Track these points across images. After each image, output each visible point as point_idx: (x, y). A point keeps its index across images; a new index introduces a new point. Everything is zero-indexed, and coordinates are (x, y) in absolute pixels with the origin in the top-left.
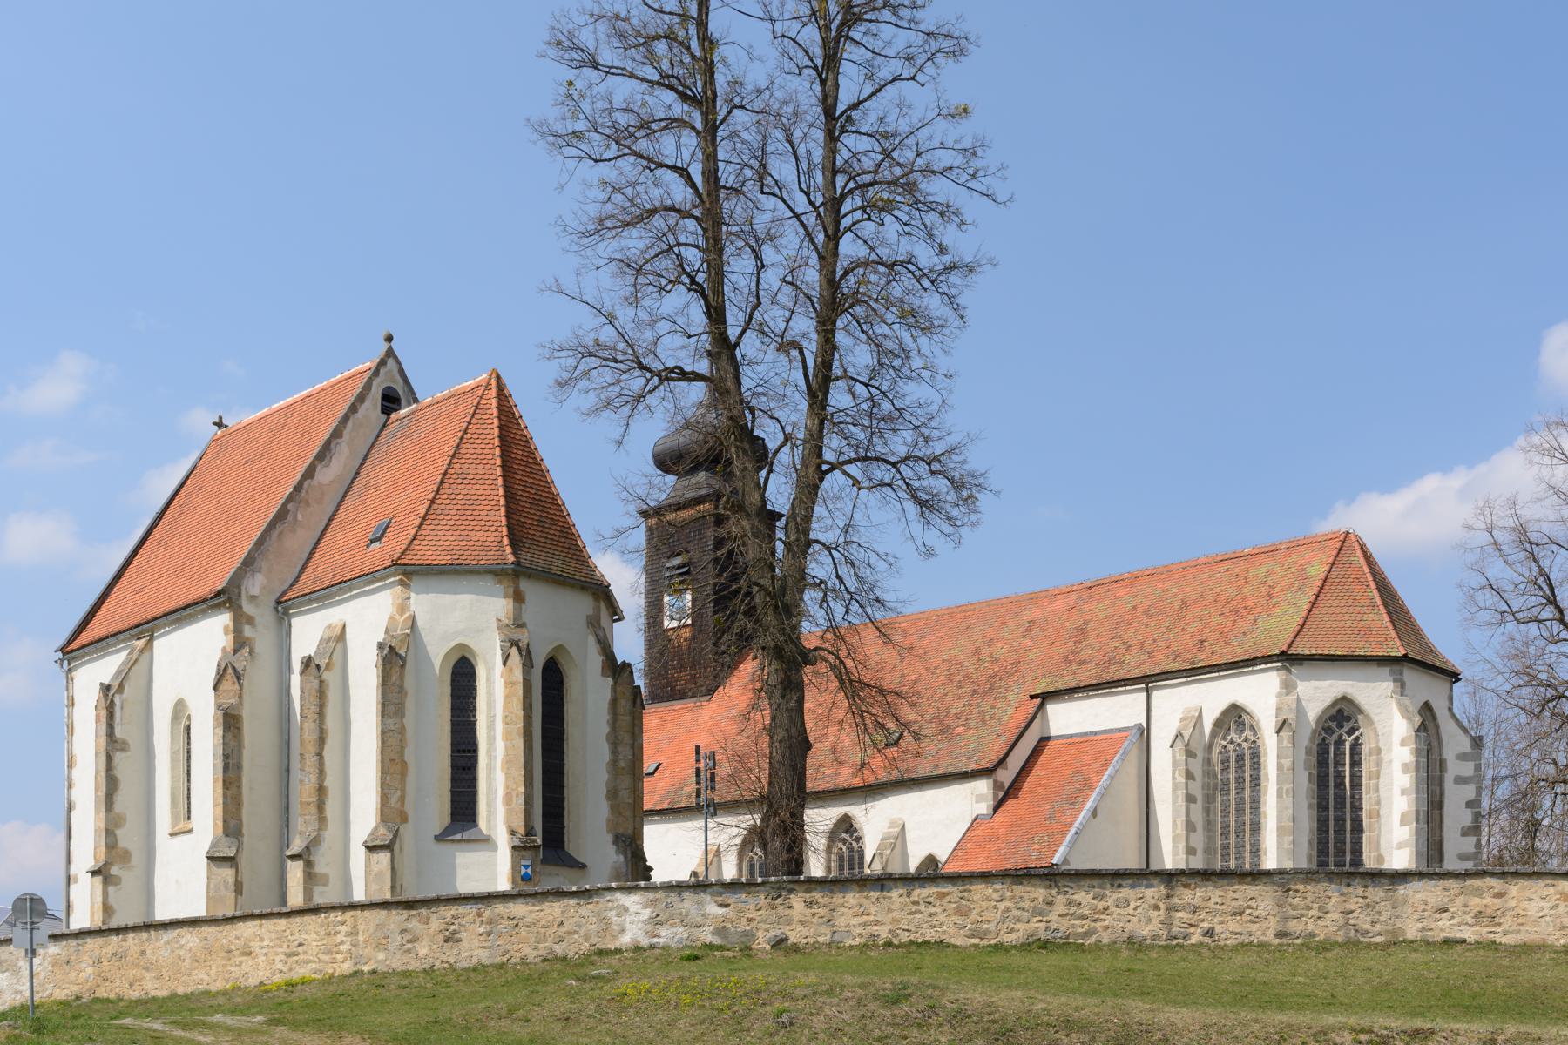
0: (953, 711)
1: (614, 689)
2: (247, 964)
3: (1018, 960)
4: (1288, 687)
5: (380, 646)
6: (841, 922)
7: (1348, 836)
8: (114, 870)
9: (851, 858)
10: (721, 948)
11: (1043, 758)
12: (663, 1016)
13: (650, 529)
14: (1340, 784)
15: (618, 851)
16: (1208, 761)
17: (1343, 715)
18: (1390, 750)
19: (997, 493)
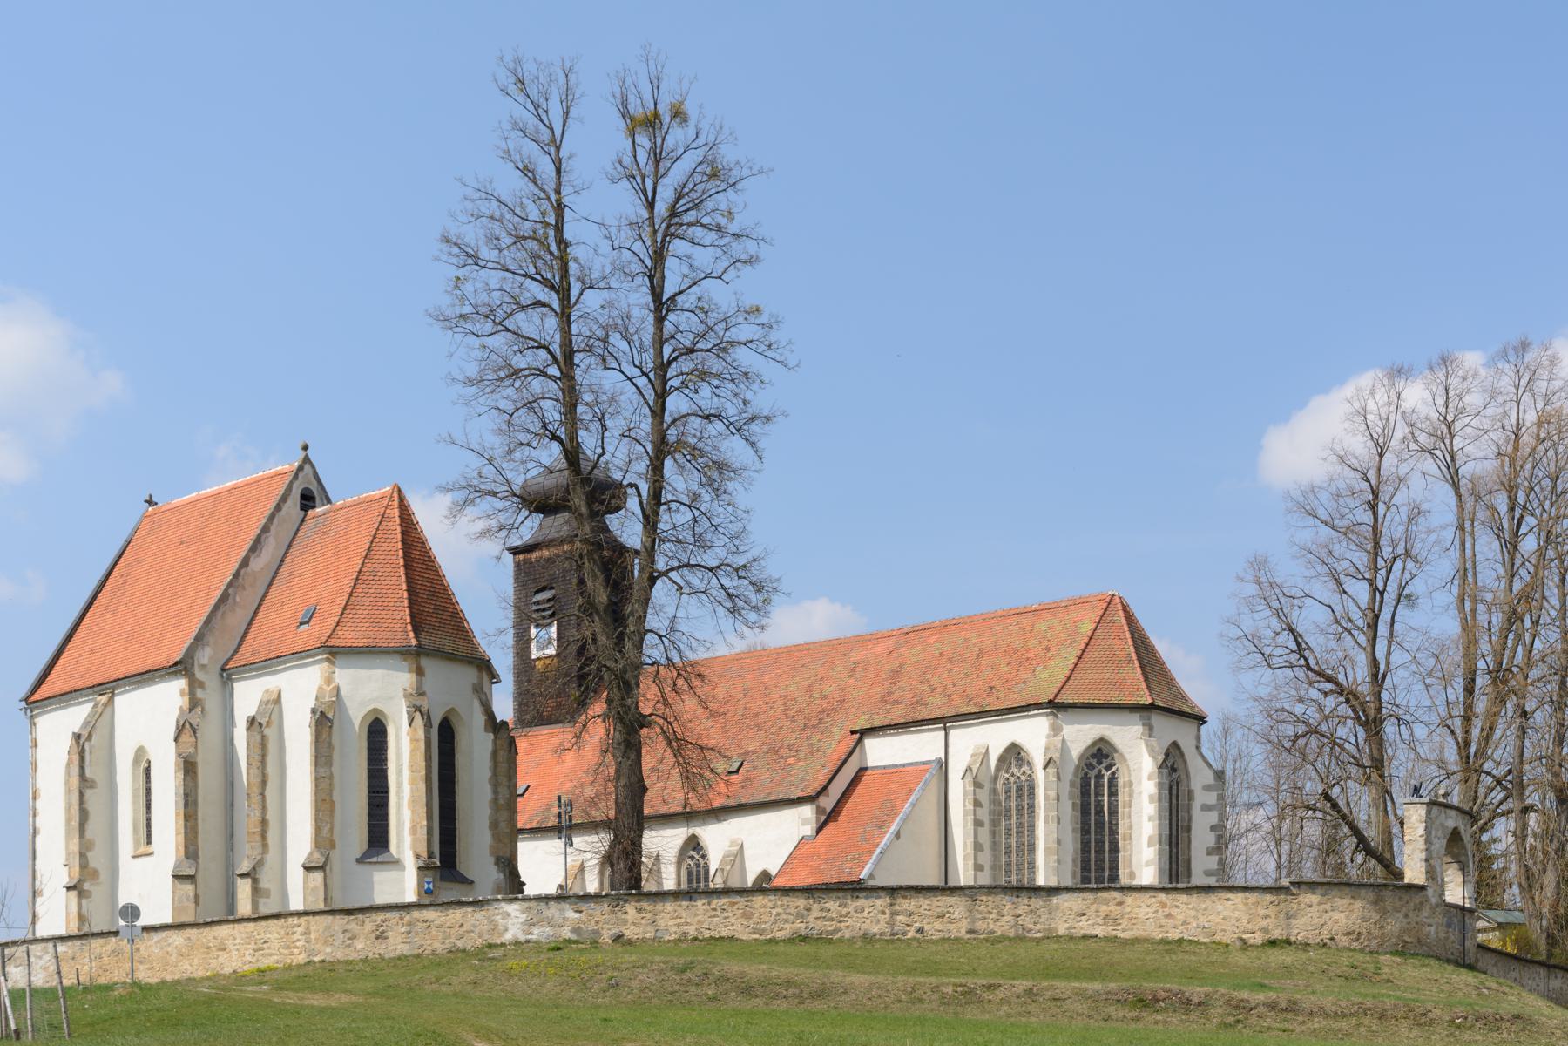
1: (495, 742)
2: (223, 957)
3: (790, 949)
4: (1055, 730)
5: (313, 711)
6: (661, 923)
8: (86, 886)
9: (698, 872)
10: (576, 942)
11: (861, 786)
12: (536, 981)
13: (517, 565)
14: (1100, 812)
16: (994, 791)
17: (1101, 753)
18: (1140, 782)
19: (788, 595)
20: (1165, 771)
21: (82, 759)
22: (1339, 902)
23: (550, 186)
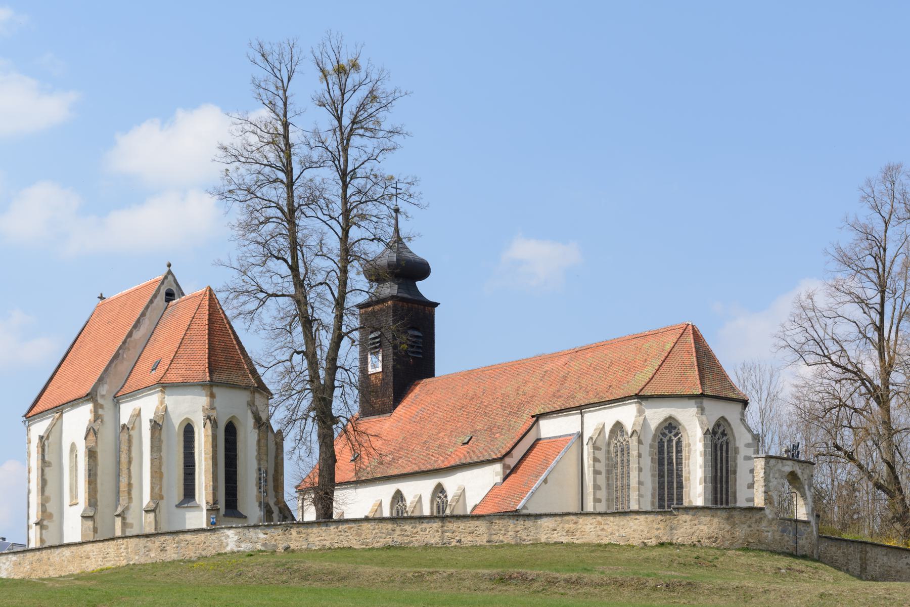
0: (498, 424)
2: (88, 561)
4: (640, 412)
5: (151, 421)
6: (311, 540)
7: (675, 491)
8: (45, 523)
10: (264, 551)
11: (535, 450)
14: (670, 463)
15: (261, 510)
16: (608, 452)
17: (671, 426)
18: (695, 444)
20: (709, 436)
21: (43, 450)
22: (703, 519)
23: (281, 113)
